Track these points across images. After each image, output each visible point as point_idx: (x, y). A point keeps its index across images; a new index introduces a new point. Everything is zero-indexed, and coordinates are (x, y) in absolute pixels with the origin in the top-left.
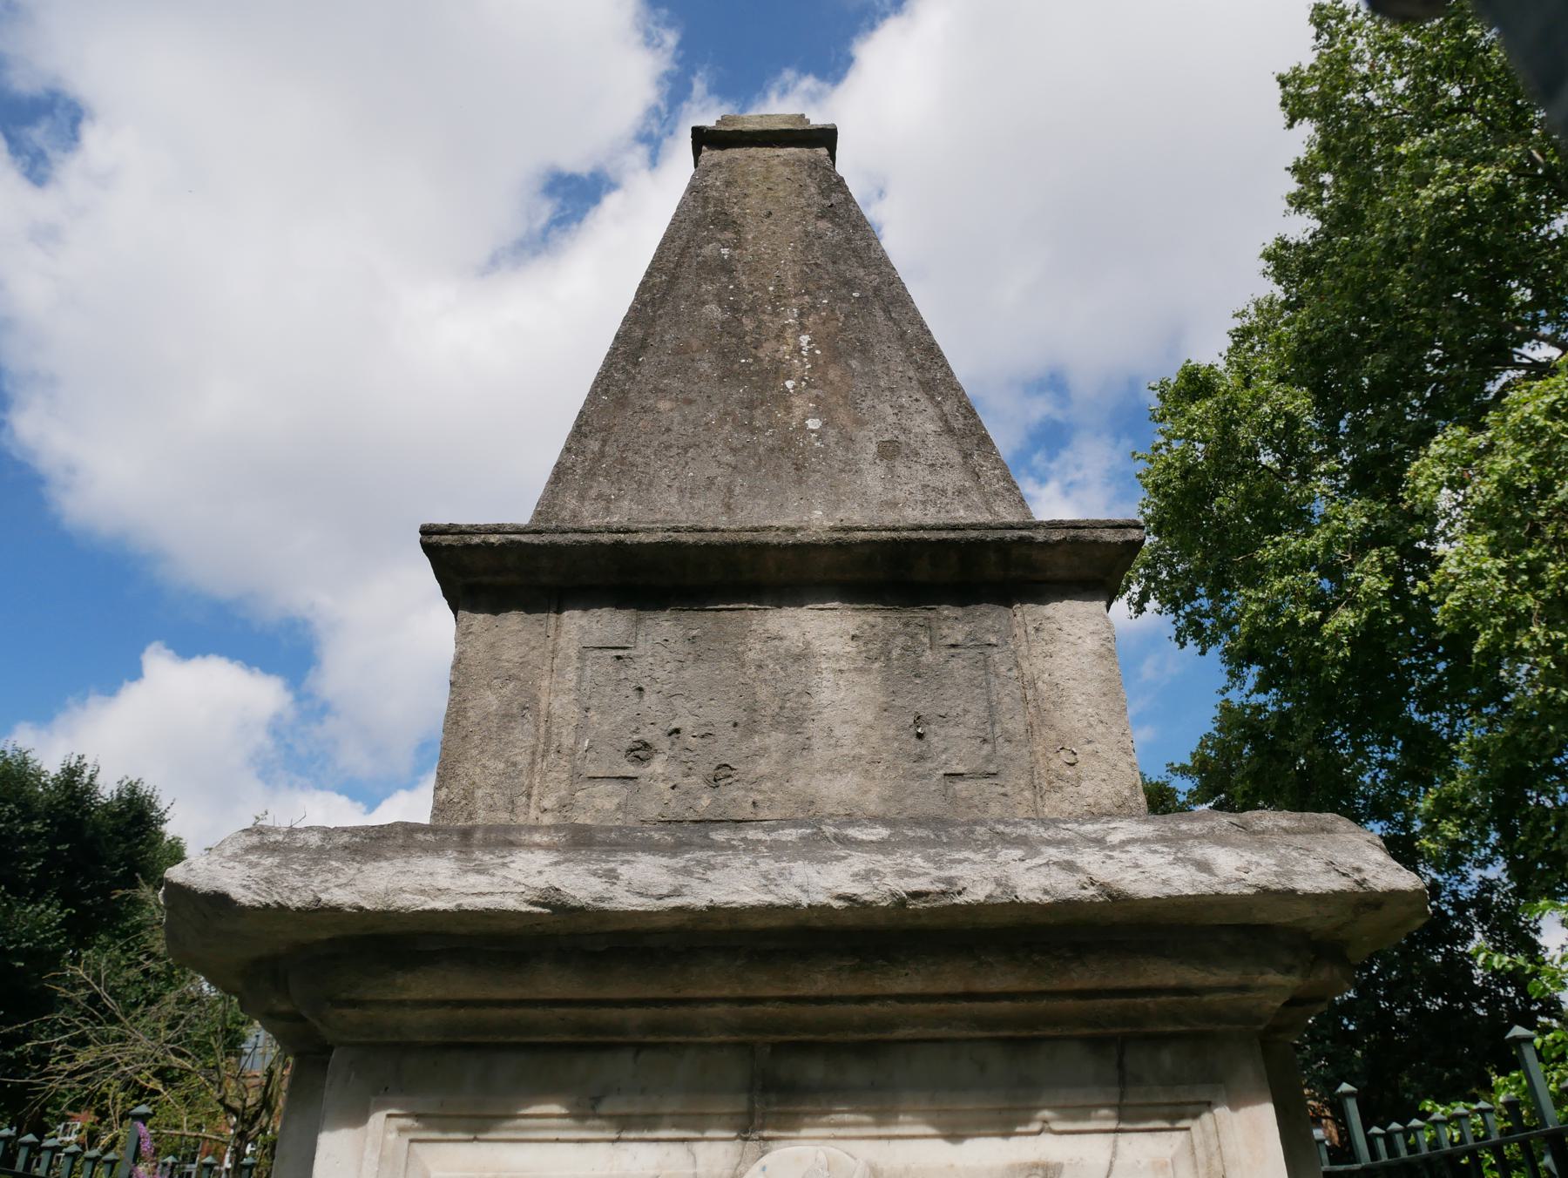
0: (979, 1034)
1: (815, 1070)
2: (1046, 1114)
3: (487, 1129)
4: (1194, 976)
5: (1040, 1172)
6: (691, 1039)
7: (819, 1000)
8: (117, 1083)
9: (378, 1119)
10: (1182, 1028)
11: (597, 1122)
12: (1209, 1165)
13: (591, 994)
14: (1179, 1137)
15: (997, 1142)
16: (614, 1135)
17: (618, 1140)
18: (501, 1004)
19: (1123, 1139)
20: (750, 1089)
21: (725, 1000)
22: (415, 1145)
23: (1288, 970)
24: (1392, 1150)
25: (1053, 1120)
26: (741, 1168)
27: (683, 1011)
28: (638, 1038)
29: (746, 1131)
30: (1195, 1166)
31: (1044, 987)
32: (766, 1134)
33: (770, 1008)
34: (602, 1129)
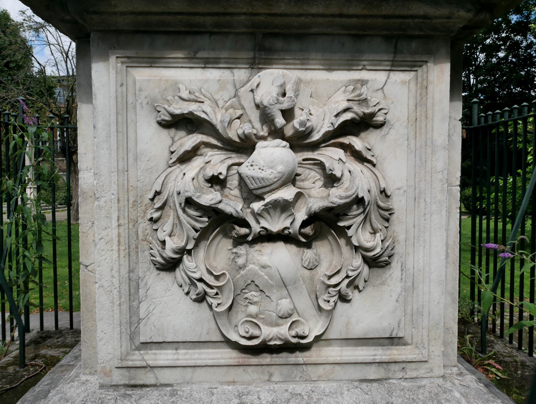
0: (343, 32)
1: (279, 44)
2: (365, 63)
3: (155, 63)
4: (431, 10)
5: (360, 82)
6: (231, 30)
7: (281, 15)
8: (9, 106)
9: (113, 59)
10: (422, 33)
11: (196, 61)
12: (422, 83)
13: (191, 10)
14: (413, 73)
15: (345, 72)
16: (203, 66)
17: (205, 67)
18: (156, 14)
19: (392, 74)
20: (254, 50)
21: (245, 14)
22: (129, 69)
23: (469, 11)
24: (486, 121)
25: (368, 65)
26: (251, 78)
27: (228, 18)
28: (210, 29)
29: (253, 65)
30: (417, 84)
31: (371, 13)
32: (260, 66)
33: (262, 18)
34: (199, 63)
